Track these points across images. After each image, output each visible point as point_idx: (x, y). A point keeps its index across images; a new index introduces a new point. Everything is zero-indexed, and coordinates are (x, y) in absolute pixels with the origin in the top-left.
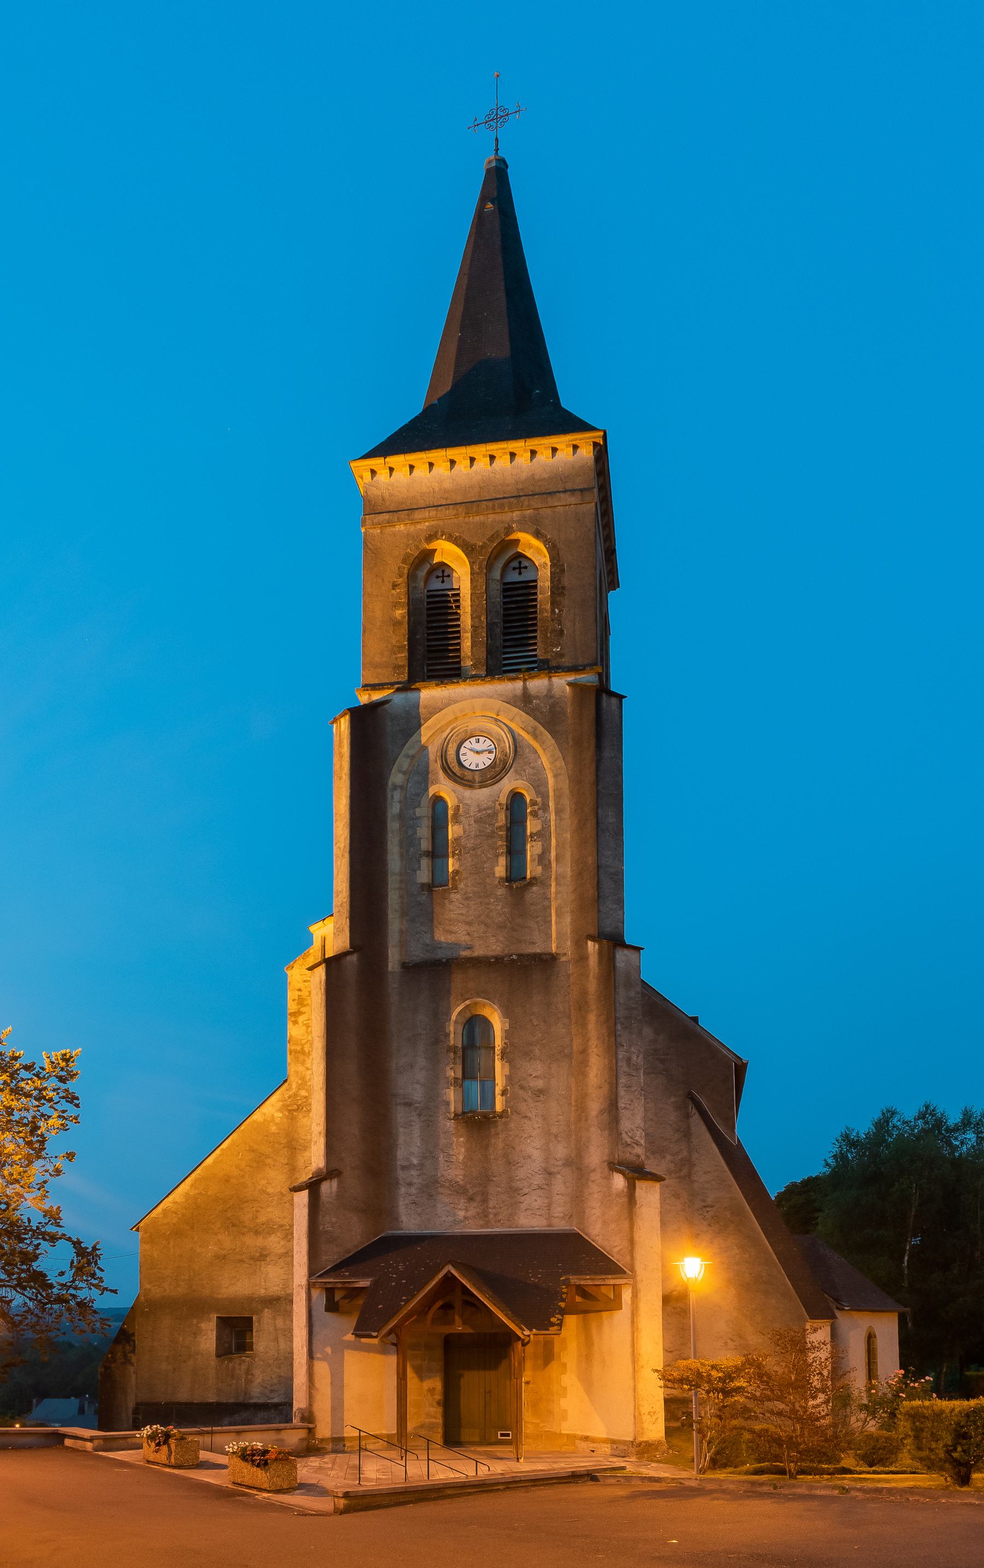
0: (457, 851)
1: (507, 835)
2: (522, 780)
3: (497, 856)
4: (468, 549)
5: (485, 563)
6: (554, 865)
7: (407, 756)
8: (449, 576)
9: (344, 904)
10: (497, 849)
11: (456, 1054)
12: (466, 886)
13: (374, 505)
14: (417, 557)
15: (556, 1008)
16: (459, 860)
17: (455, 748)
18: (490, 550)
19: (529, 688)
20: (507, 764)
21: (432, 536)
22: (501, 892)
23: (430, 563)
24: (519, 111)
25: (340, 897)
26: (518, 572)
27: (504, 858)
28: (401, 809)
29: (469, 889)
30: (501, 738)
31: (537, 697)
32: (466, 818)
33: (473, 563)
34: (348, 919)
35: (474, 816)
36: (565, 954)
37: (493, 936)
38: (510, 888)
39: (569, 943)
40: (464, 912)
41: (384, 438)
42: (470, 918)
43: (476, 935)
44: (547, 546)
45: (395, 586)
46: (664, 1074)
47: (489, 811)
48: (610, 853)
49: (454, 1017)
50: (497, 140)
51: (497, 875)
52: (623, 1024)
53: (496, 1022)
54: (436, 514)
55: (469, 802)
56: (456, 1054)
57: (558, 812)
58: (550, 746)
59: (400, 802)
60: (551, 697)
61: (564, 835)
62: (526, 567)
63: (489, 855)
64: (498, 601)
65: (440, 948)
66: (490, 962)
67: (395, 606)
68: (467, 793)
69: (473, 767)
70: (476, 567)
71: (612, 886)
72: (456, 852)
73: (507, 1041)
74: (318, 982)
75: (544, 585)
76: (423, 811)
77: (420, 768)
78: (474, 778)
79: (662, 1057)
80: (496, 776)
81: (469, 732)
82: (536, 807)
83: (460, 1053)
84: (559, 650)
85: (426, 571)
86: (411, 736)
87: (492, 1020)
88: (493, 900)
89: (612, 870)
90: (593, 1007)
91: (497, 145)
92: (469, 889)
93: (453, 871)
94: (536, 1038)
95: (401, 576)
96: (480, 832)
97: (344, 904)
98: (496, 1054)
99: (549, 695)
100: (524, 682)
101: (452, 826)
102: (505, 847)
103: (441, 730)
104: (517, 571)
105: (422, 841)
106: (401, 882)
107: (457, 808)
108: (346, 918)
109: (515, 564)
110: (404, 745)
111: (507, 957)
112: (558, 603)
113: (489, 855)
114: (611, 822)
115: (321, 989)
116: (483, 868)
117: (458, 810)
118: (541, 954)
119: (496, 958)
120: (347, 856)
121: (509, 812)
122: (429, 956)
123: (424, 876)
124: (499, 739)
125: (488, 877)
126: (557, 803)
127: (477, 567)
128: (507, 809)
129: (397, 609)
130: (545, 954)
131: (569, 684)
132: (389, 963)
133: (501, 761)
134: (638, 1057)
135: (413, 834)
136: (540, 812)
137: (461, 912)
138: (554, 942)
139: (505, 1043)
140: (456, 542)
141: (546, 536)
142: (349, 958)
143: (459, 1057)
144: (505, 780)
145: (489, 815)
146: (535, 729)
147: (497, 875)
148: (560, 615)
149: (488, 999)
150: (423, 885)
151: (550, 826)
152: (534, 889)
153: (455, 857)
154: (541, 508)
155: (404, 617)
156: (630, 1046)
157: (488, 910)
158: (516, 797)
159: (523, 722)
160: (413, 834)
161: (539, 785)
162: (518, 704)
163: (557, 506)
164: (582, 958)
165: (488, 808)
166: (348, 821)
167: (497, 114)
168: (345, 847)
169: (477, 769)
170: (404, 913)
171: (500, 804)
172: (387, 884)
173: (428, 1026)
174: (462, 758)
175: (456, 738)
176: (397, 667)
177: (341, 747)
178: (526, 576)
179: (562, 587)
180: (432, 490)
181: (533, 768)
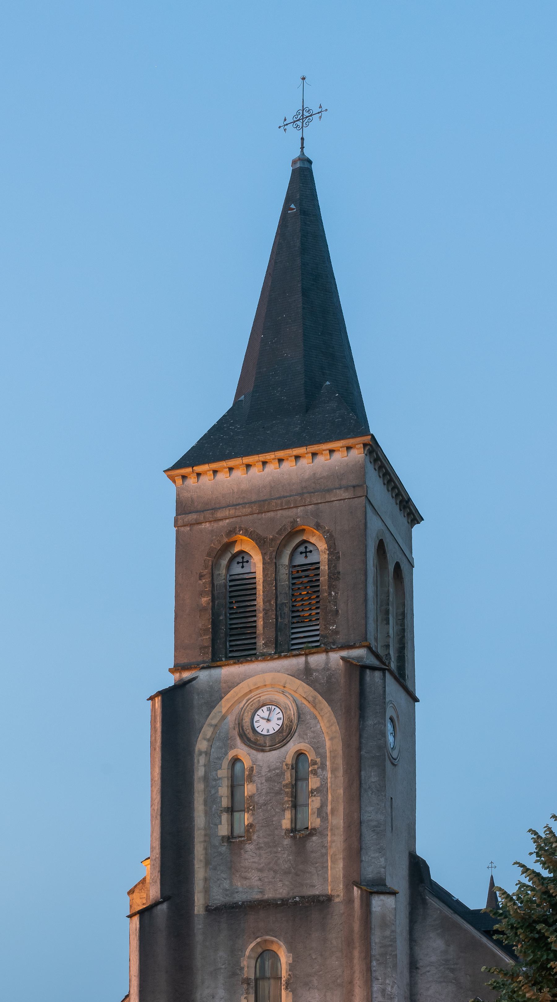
0: (251, 806)
1: (292, 792)
2: (305, 743)
3: (284, 810)
4: (261, 542)
5: (274, 553)
6: (330, 817)
7: (210, 725)
8: (247, 562)
9: (157, 860)
10: (283, 804)
11: (250, 985)
12: (258, 837)
13: (185, 506)
14: (219, 550)
15: (331, 943)
16: (253, 814)
17: (250, 717)
18: (278, 542)
19: (310, 662)
20: (292, 729)
21: (232, 531)
22: (287, 842)
23: (231, 553)
24: (321, 112)
25: (154, 852)
26: (305, 555)
27: (290, 812)
28: (205, 772)
29: (261, 841)
30: (287, 707)
31: (317, 670)
32: (259, 777)
33: (265, 554)
34: (159, 873)
35: (265, 776)
36: (338, 896)
37: (280, 881)
38: (294, 838)
39: (341, 886)
40: (256, 860)
41: (193, 442)
42: (262, 865)
43: (266, 880)
44: (325, 536)
45: (201, 577)
46: (453, 983)
47: (277, 771)
48: (372, 808)
49: (247, 953)
50: (302, 139)
51: (284, 827)
52: (378, 960)
53: (282, 956)
54: (235, 512)
55: (261, 764)
56: (250, 985)
57: (334, 770)
58: (327, 713)
59: (205, 766)
60: (328, 669)
61: (338, 791)
62: (311, 551)
63: (277, 810)
64: (286, 584)
65: (237, 892)
66: (277, 904)
67: (201, 595)
68: (260, 755)
69: (265, 733)
70: (267, 558)
71: (374, 837)
72: (250, 808)
73: (290, 973)
74: (135, 928)
75: (324, 568)
76: (223, 772)
77: (222, 735)
78: (265, 743)
79: (452, 967)
80: (283, 740)
81: (261, 702)
82: (316, 766)
83: (253, 984)
84: (334, 628)
85: (227, 559)
86: (214, 707)
87: (279, 953)
88: (280, 849)
89: (374, 823)
90: (357, 944)
91: (302, 144)
92: (261, 841)
93: (248, 825)
94: (314, 970)
95: (206, 568)
96: (270, 789)
97: (157, 860)
98: (282, 984)
99: (326, 668)
100: (306, 657)
101: (247, 785)
102: (290, 803)
103: (239, 701)
104: (304, 555)
105: (222, 799)
106: (205, 835)
107: (251, 769)
108: (158, 872)
109: (302, 549)
110: (208, 716)
111: (292, 899)
112: (334, 587)
113: (277, 810)
114: (374, 781)
115: (136, 935)
116: (273, 821)
117: (253, 771)
118: (319, 896)
119: (282, 900)
120: (159, 817)
121: (294, 771)
122: (227, 900)
123: (223, 830)
124: (286, 707)
125: (277, 829)
126: (332, 763)
127: (268, 557)
128: (292, 769)
129: (203, 597)
130: (323, 896)
131: (343, 658)
132: (196, 907)
133: (287, 726)
134: (392, 987)
135: (216, 793)
136: (319, 771)
137: (254, 860)
138: (330, 885)
139: (289, 975)
140: (251, 536)
141: (325, 528)
142: (159, 907)
143: (252, 987)
144: (291, 744)
145: (277, 775)
146: (315, 698)
147: (284, 827)
148: (336, 597)
149: (275, 937)
150: (223, 837)
151: (327, 783)
152: (314, 838)
153: (250, 812)
154: (321, 503)
155: (208, 604)
156: (385, 979)
157: (276, 858)
158: (300, 755)
159: (305, 692)
160: (216, 793)
161: (318, 747)
162: (301, 676)
163: (334, 501)
164: (350, 901)
165: (277, 768)
166: (160, 788)
167: (303, 115)
168: (158, 810)
169: (268, 734)
170: (207, 863)
171: (286, 765)
172: (194, 838)
173: (226, 961)
174: (256, 725)
175: (251, 708)
176: (202, 648)
177: (156, 722)
178: (312, 558)
179: (337, 572)
180: (232, 491)
181: (313, 732)
